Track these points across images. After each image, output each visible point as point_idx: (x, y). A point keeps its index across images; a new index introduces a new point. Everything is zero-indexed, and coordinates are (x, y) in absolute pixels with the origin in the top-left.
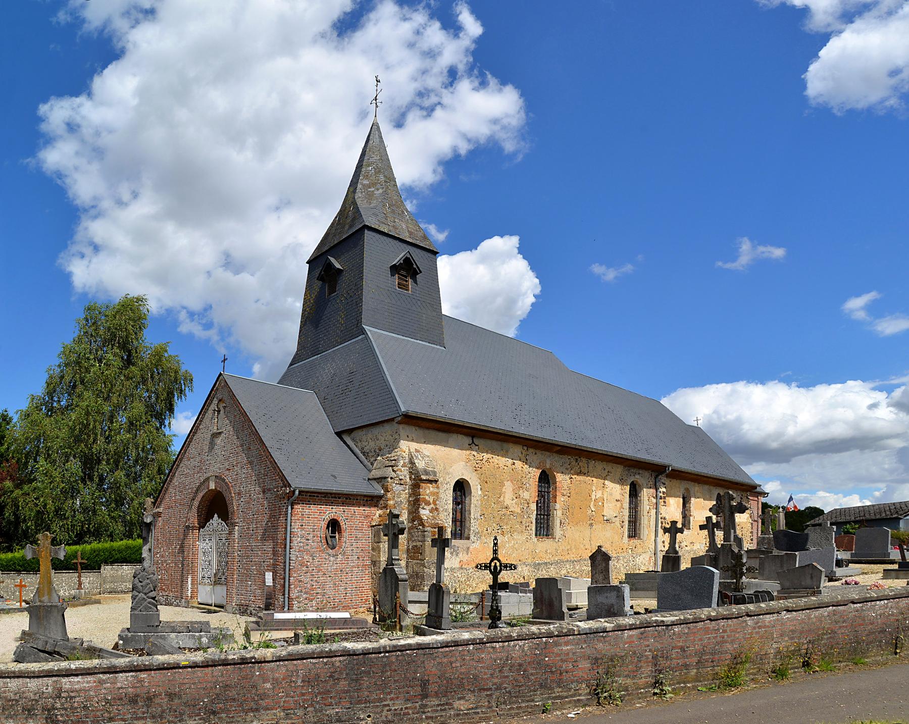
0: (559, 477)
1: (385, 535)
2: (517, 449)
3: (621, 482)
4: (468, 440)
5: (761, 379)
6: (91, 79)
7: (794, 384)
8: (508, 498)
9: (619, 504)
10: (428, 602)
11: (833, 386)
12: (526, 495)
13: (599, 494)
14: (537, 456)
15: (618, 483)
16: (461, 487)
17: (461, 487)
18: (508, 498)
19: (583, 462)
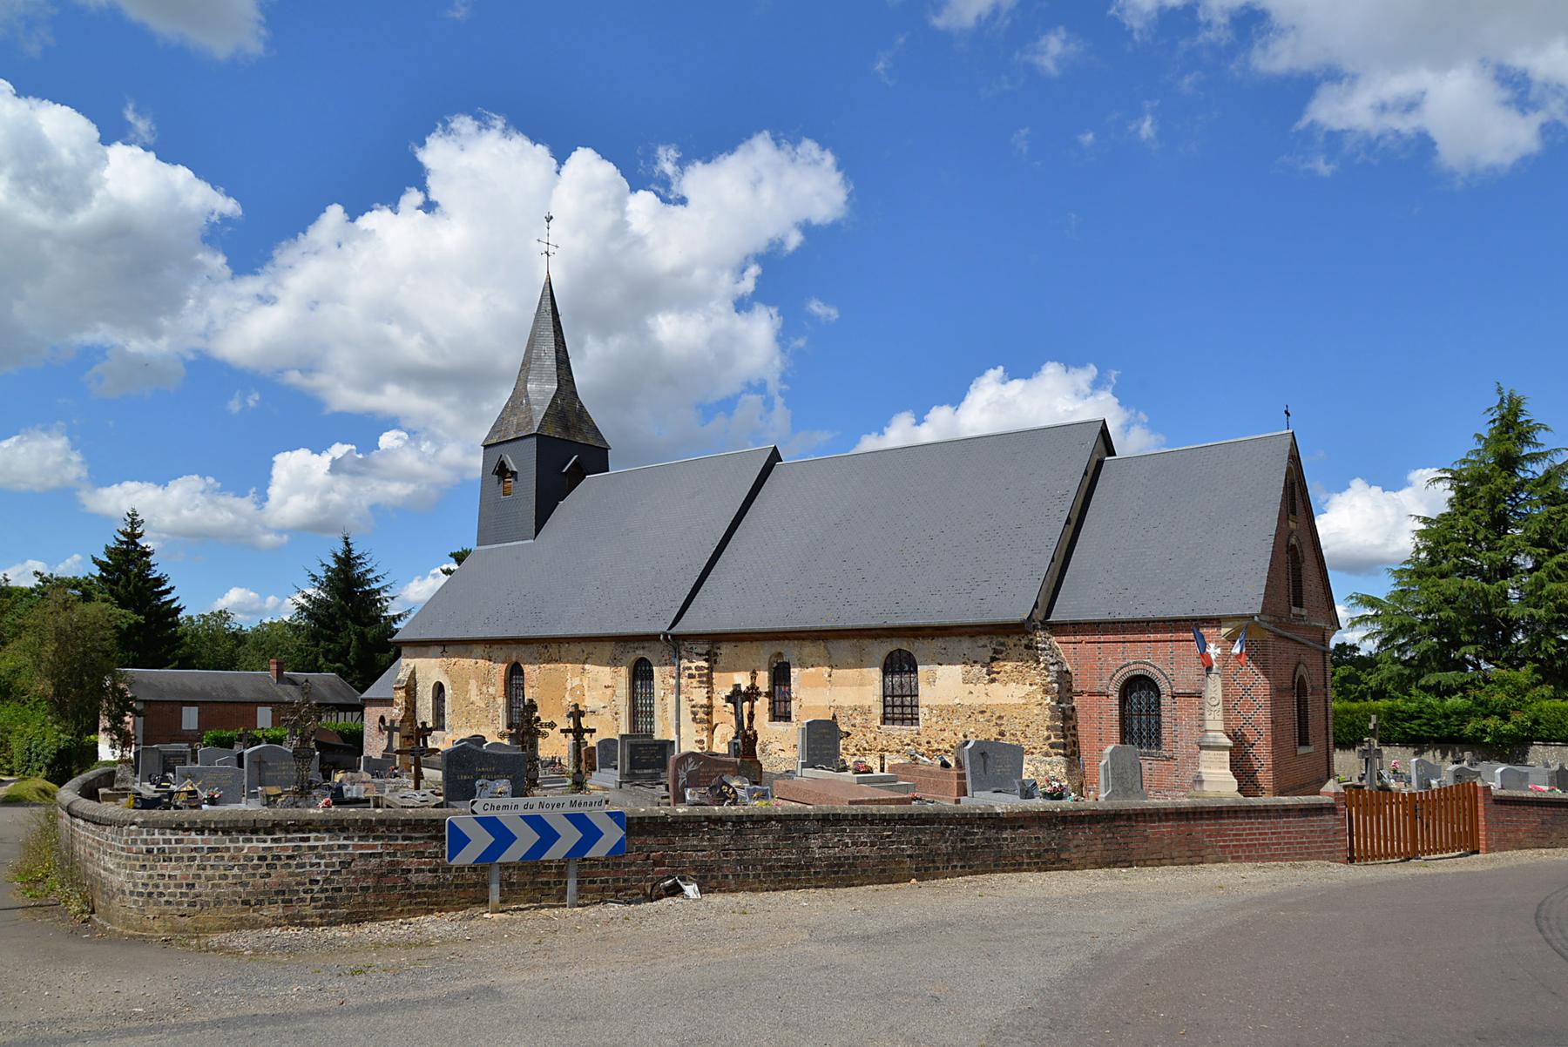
0: (527, 668)
1: (320, 719)
2: (479, 649)
3: (614, 662)
4: (440, 649)
5: (109, 485)
6: (819, 226)
7: (794, 240)
8: (473, 694)
9: (609, 691)
10: (1230, 749)
11: (605, 162)
12: (492, 690)
13: (576, 681)
14: (497, 651)
15: (608, 664)
16: (439, 688)
17: (439, 688)
18: (473, 694)
19: (554, 649)
